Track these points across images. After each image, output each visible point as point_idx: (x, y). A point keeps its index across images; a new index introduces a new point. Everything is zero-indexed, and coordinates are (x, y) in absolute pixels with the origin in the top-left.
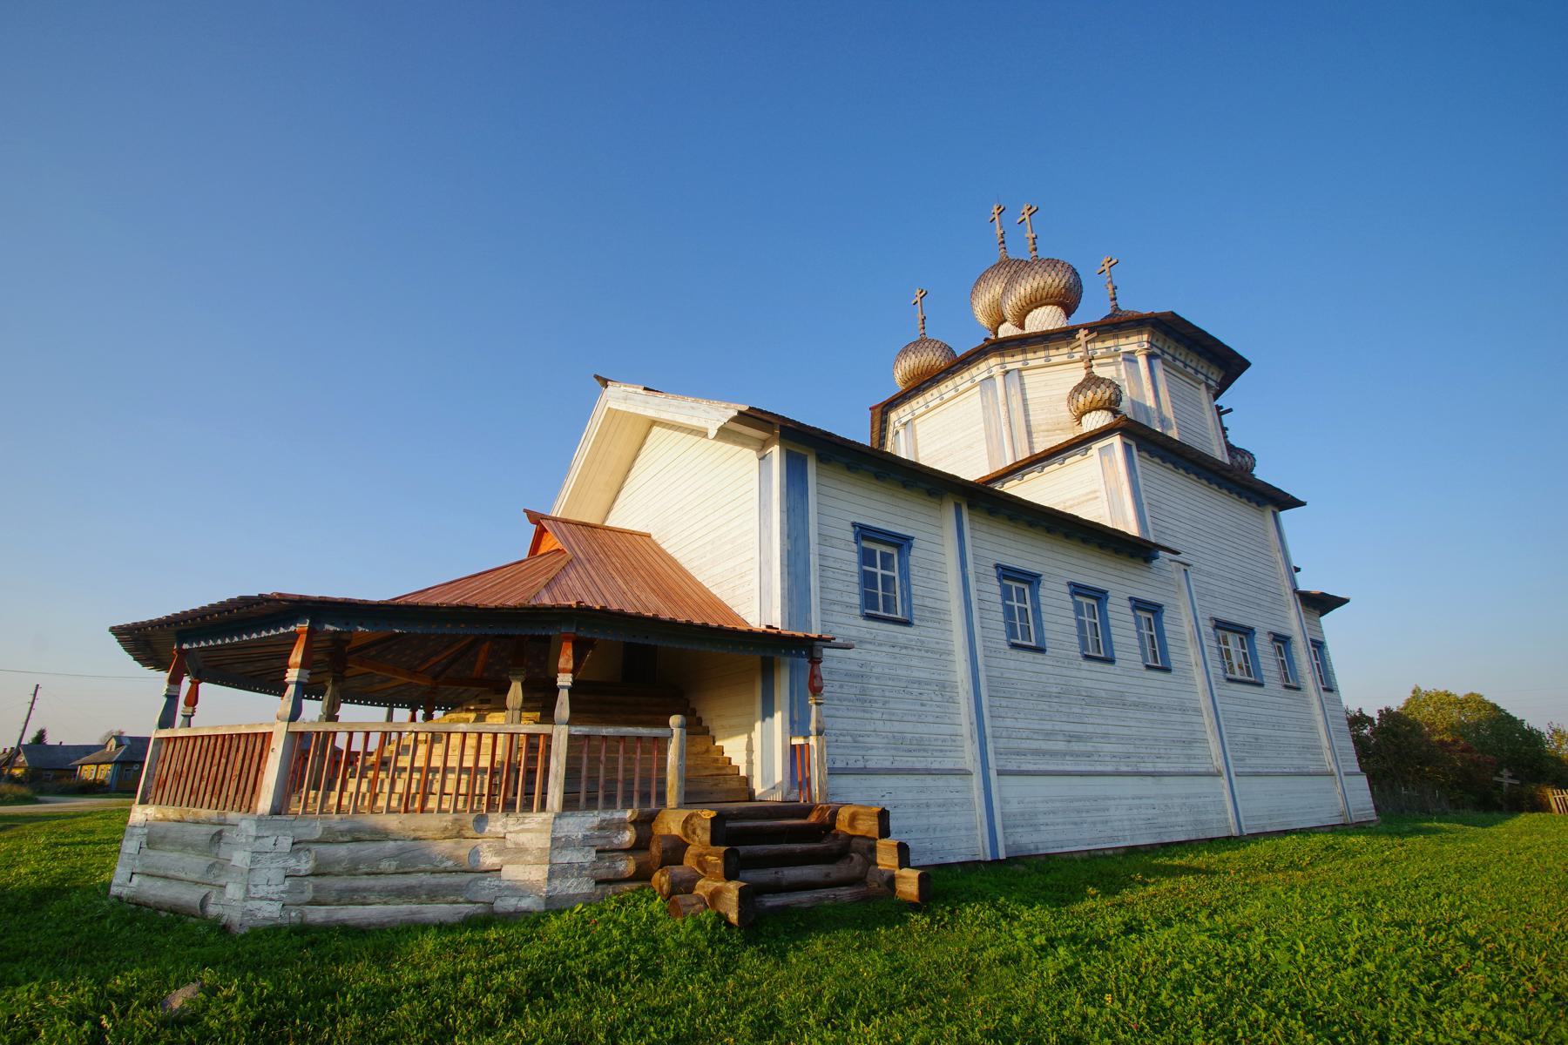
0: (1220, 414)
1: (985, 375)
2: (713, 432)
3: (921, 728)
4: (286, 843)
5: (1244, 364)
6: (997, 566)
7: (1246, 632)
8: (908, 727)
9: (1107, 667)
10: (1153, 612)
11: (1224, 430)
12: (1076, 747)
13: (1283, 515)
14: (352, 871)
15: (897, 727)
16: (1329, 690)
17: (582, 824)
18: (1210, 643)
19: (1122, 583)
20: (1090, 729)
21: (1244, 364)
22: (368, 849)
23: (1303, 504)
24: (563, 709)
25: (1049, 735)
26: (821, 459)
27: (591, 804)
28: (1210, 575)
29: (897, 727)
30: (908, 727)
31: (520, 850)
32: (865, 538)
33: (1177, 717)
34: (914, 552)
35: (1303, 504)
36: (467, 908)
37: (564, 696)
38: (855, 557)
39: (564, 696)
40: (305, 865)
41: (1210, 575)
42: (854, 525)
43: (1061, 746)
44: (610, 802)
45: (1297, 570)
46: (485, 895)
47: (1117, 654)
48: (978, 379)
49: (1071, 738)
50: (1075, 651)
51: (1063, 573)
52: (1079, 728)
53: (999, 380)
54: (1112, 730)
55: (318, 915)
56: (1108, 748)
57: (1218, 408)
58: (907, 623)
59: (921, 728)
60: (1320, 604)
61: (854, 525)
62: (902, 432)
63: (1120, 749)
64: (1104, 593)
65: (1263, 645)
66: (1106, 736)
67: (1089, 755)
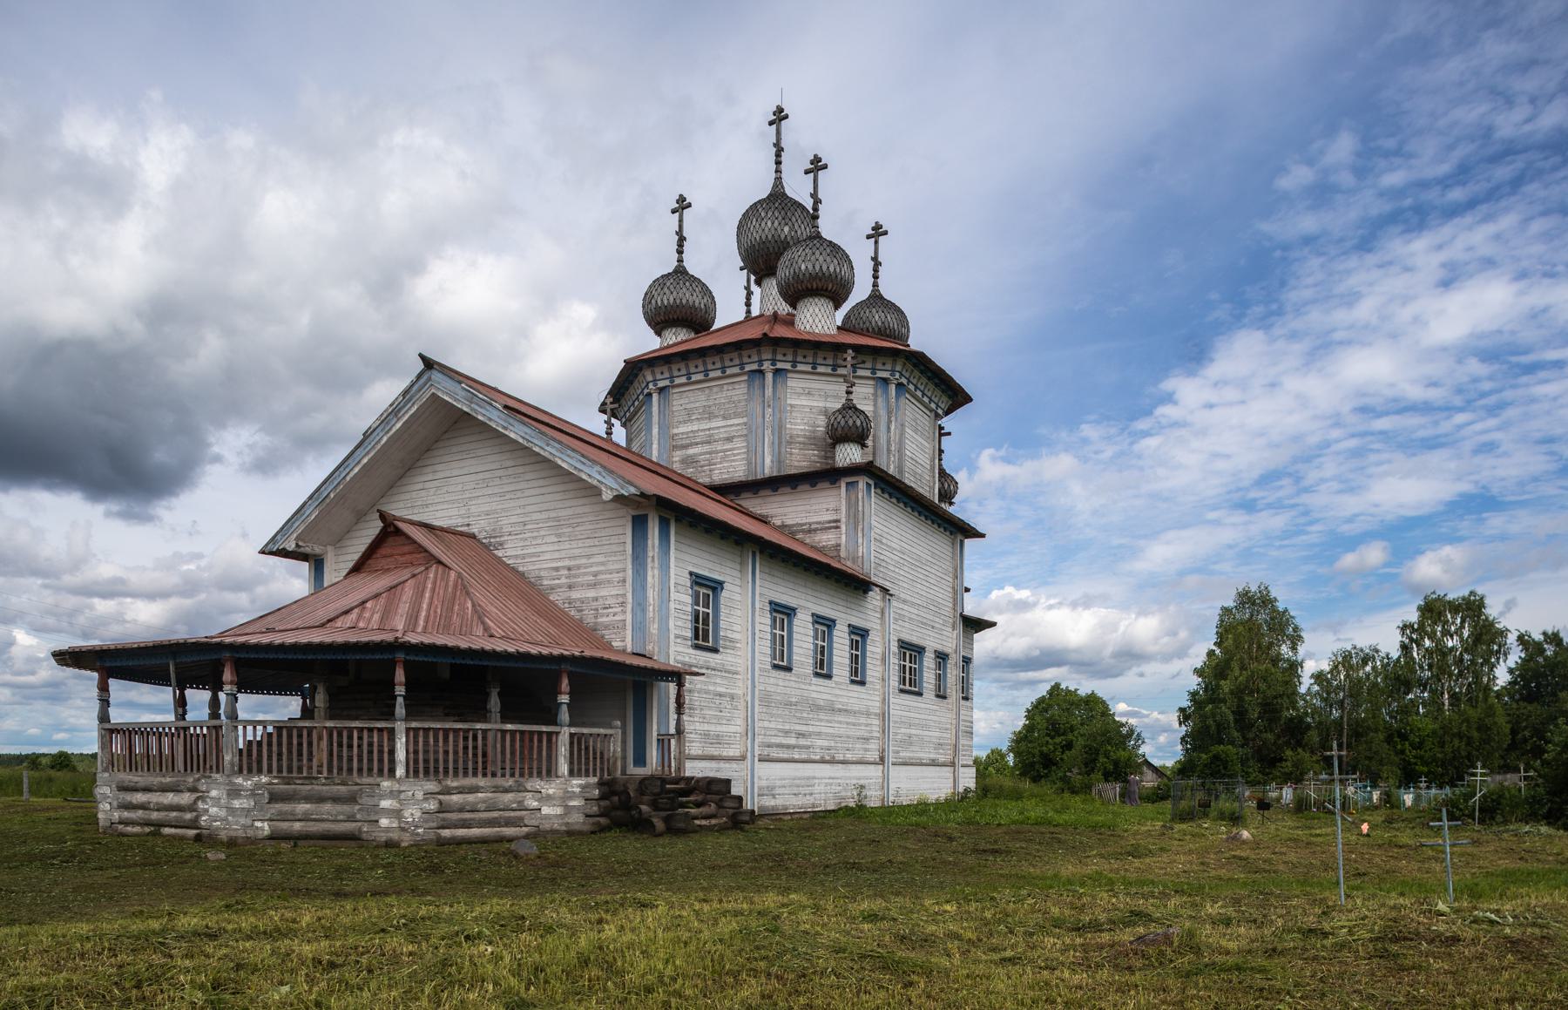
0: (941, 435)
1: (755, 367)
2: (607, 495)
3: (719, 728)
4: (420, 795)
5: (967, 399)
6: (771, 603)
7: (920, 650)
8: (712, 728)
9: (827, 682)
10: (714, 589)
11: (941, 451)
12: (802, 742)
13: (967, 542)
14: (461, 810)
15: (706, 727)
16: (966, 698)
17: (577, 783)
18: (894, 661)
19: (808, 601)
20: (811, 729)
21: (967, 399)
22: (471, 798)
23: (983, 536)
24: (400, 710)
25: (787, 733)
26: (677, 520)
27: (579, 775)
28: (905, 601)
29: (706, 727)
30: (712, 728)
31: (549, 797)
32: (697, 584)
33: (863, 720)
34: (724, 594)
35: (983, 536)
36: (525, 829)
37: (400, 700)
38: (689, 600)
39: (400, 700)
40: (432, 805)
41: (905, 601)
42: (691, 574)
43: (792, 741)
44: (587, 775)
45: (967, 590)
46: (534, 823)
47: (835, 671)
48: (748, 368)
49: (800, 735)
50: (809, 670)
51: (809, 605)
52: (804, 728)
53: (769, 376)
54: (824, 730)
55: (446, 833)
56: (820, 743)
57: (941, 428)
58: (715, 650)
59: (719, 728)
60: (974, 625)
61: (691, 574)
62: (655, 397)
63: (825, 743)
64: (834, 621)
65: (929, 661)
66: (819, 734)
67: (808, 747)
